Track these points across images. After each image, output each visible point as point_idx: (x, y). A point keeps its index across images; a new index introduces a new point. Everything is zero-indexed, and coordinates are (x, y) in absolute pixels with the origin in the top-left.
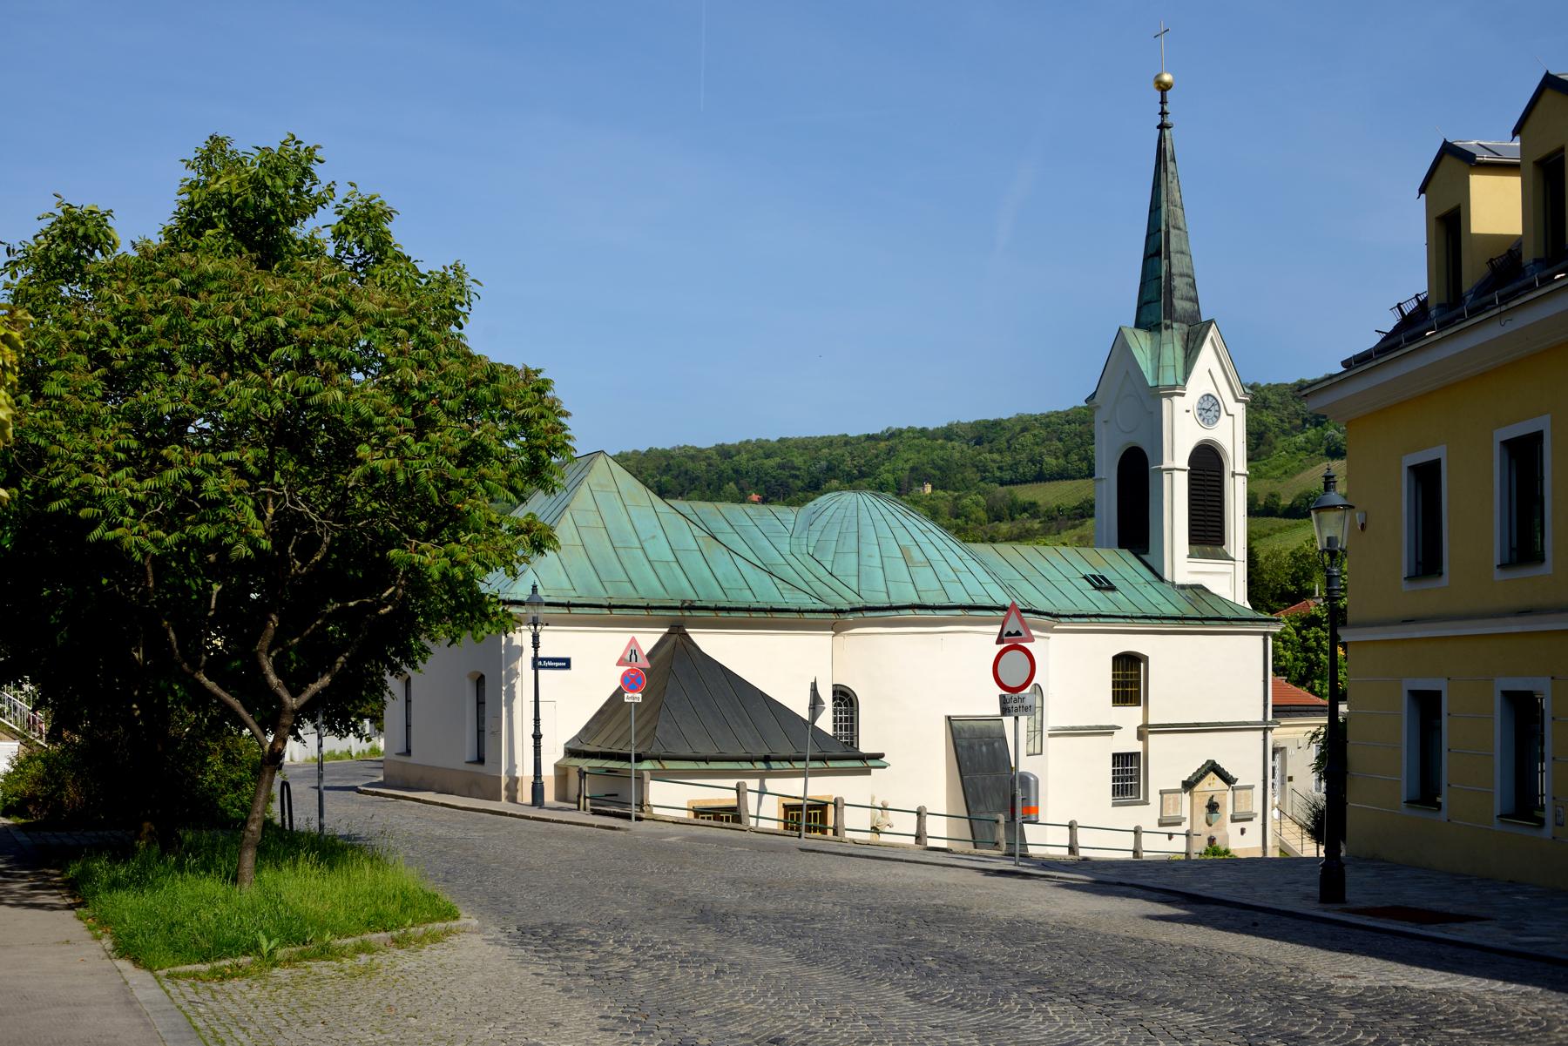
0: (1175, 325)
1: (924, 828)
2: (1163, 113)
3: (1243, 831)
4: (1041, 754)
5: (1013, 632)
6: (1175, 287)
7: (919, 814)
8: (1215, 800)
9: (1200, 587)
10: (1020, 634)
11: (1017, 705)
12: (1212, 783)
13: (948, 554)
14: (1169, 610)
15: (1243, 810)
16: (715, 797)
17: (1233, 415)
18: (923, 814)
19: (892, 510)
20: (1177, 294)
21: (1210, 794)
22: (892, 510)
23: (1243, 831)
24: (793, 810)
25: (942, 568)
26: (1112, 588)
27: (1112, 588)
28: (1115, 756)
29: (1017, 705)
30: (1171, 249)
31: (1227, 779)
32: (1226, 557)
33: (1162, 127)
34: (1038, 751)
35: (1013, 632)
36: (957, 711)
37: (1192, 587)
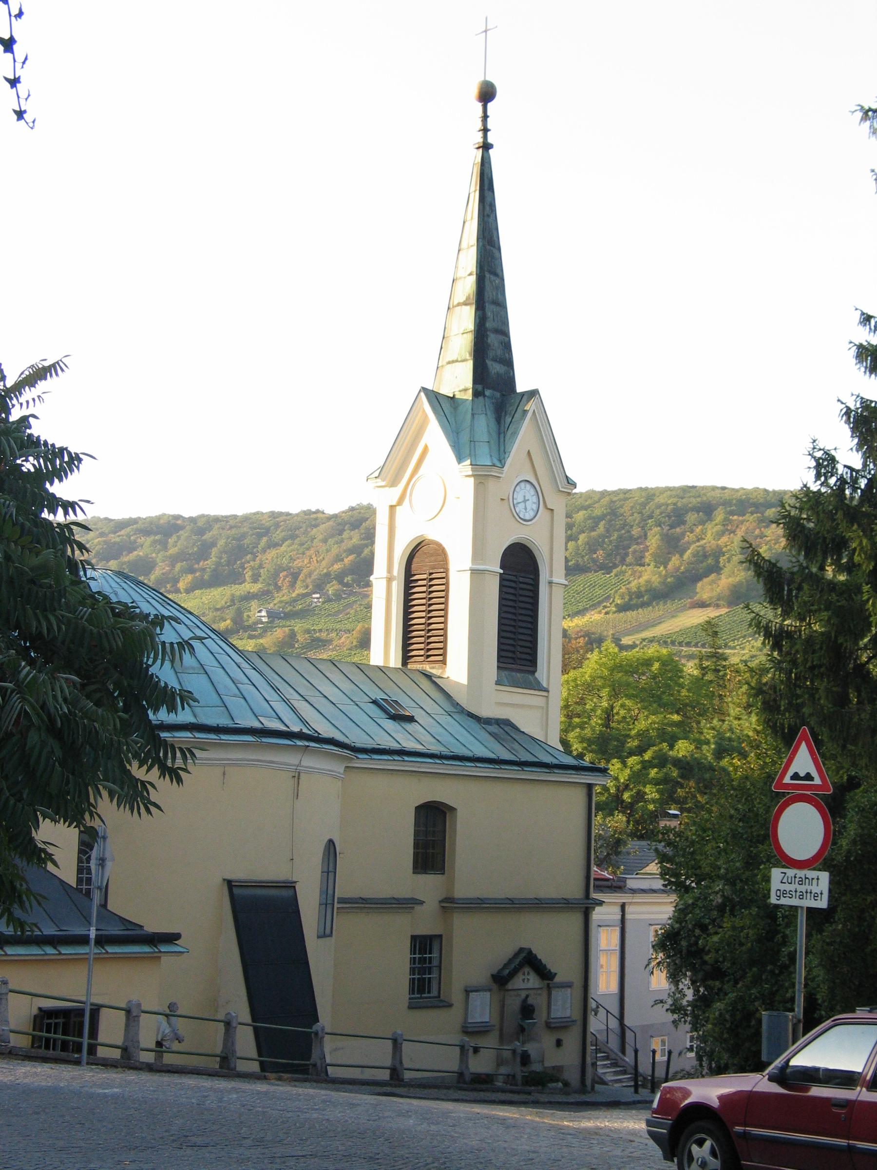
0: (488, 393)
1: (233, 1044)
2: (485, 130)
3: (559, 1043)
4: (331, 935)
5: (802, 774)
6: (489, 346)
7: (128, 1012)
8: (530, 1001)
9: (508, 723)
10: (812, 779)
11: (803, 888)
12: (527, 981)
13: (224, 659)
14: (480, 751)
15: (559, 1014)
16: (61, 1005)
17: (552, 510)
18: (399, 1041)
19: (146, 596)
20: (491, 354)
21: (523, 994)
22: (146, 596)
23: (559, 1043)
24: (49, 1017)
25: (218, 675)
26: (411, 719)
27: (411, 719)
28: (414, 938)
29: (803, 888)
30: (486, 298)
31: (544, 973)
32: (537, 686)
33: (486, 147)
34: (328, 931)
35: (802, 774)
36: (239, 874)
37: (499, 722)
